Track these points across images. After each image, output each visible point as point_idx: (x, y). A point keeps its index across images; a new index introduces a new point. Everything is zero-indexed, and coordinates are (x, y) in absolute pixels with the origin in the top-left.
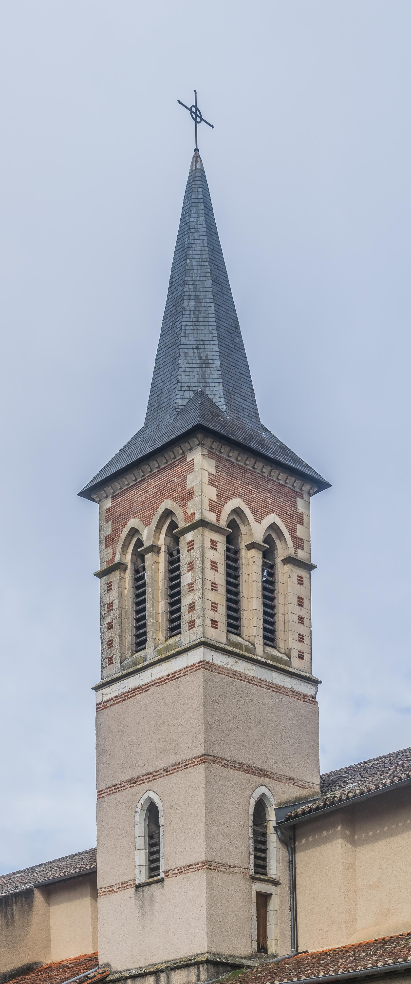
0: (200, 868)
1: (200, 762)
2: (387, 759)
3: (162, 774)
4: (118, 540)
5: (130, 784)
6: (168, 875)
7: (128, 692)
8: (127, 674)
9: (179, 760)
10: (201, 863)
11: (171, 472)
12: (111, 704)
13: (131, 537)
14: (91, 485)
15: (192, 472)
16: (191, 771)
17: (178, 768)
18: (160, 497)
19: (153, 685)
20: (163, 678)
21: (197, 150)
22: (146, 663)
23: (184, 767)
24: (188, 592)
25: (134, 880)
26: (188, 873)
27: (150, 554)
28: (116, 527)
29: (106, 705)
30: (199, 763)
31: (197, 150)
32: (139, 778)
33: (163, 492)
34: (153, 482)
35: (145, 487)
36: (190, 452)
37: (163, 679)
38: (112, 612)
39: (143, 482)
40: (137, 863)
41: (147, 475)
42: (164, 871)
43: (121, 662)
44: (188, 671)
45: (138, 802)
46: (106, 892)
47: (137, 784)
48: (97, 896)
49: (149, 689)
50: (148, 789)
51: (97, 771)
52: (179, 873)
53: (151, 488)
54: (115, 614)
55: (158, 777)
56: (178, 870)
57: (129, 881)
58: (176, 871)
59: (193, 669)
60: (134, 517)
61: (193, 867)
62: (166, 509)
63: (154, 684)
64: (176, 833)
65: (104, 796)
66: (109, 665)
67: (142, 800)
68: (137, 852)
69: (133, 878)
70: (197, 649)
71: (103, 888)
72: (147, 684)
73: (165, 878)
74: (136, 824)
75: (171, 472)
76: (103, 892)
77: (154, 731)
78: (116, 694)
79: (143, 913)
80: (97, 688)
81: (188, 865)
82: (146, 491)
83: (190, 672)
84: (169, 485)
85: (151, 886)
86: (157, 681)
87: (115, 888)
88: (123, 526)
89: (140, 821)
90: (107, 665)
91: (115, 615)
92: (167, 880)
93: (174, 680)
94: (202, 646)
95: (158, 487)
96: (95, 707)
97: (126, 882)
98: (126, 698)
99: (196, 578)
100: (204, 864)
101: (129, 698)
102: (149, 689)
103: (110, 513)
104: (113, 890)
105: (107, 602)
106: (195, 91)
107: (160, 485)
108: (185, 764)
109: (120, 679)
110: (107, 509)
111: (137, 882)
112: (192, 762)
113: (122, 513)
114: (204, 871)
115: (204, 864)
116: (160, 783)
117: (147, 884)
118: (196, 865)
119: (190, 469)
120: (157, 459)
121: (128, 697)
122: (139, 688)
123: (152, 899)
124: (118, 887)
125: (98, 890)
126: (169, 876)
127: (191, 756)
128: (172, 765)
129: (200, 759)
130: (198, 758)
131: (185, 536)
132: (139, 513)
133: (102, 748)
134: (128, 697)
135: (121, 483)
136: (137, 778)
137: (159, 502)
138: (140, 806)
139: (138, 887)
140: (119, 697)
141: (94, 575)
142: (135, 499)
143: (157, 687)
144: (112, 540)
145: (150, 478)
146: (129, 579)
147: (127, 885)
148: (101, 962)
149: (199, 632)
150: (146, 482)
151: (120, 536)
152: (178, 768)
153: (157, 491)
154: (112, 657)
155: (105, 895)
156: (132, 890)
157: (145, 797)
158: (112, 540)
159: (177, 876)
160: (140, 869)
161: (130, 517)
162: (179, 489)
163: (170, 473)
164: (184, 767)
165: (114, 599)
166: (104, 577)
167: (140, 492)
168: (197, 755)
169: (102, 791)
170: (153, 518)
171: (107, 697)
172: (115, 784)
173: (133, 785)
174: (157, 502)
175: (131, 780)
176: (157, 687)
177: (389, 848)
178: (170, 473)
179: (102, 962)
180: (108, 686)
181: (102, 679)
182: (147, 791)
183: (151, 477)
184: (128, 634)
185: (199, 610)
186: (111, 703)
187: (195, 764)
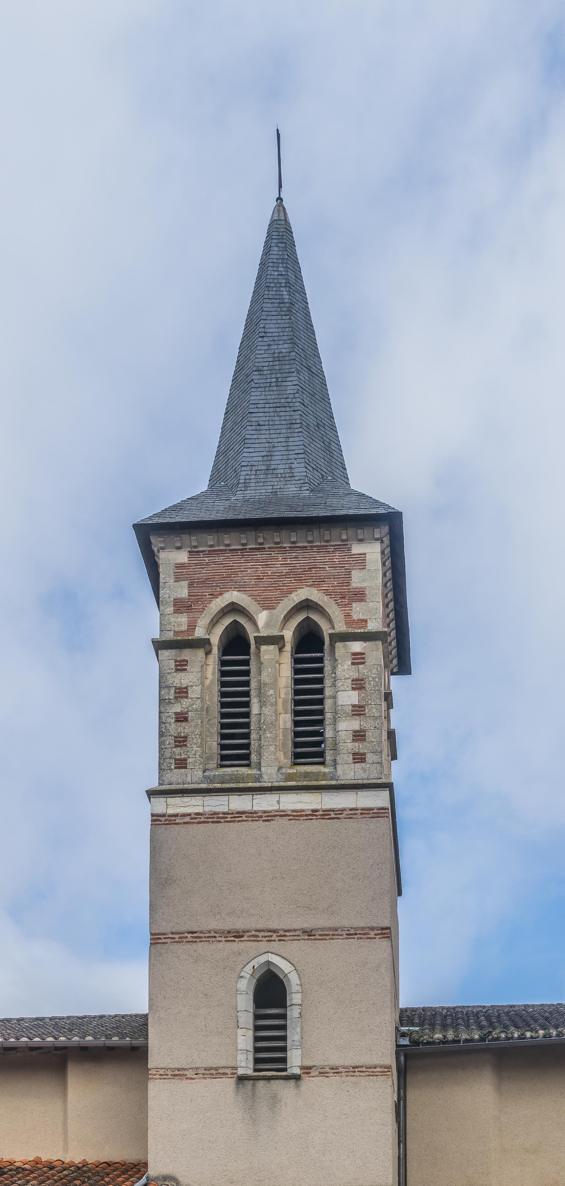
0: (378, 1074)
1: (380, 936)
2: (42, 1024)
3: (298, 936)
4: (202, 610)
5: (227, 937)
6: (310, 1073)
7: (224, 813)
8: (192, 789)
9: (337, 925)
10: (381, 1067)
11: (319, 557)
12: (185, 820)
13: (222, 614)
14: (156, 521)
15: (363, 569)
16: (362, 944)
17: (333, 935)
18: (294, 580)
19: (281, 816)
20: (303, 811)
21: (279, 199)
22: (257, 785)
23: (345, 936)
24: (353, 715)
25: (236, 1068)
26: (351, 1076)
27: (272, 647)
28: (194, 593)
29: (175, 820)
30: (378, 937)
31: (279, 199)
32: (248, 932)
33: (302, 577)
34: (281, 558)
35: (262, 560)
36: (360, 544)
37: (304, 813)
38: (186, 700)
39: (259, 552)
40: (240, 1047)
41: (268, 546)
42: (300, 1065)
43: (204, 772)
44: (357, 814)
45: (246, 964)
46: (167, 1075)
47: (242, 939)
48: (147, 1080)
49: (272, 820)
50: (268, 950)
51: (151, 905)
52: (333, 1073)
53: (277, 564)
54: (193, 705)
55: (288, 938)
56: (332, 1069)
57: (223, 1067)
58: (327, 1070)
59: (369, 814)
60: (238, 591)
61: (364, 1069)
62: (307, 600)
63: (282, 814)
64: (329, 1019)
65: (167, 943)
66: (176, 768)
67: (256, 963)
68: (240, 1032)
69: (233, 1065)
70: (376, 791)
71: (162, 1069)
72: (270, 812)
73: (302, 1075)
74: (239, 992)
75: (319, 557)
76: (161, 1075)
77: (284, 876)
78: (200, 810)
79: (254, 1117)
80: (151, 794)
81: (353, 1065)
82: (265, 565)
83: (361, 816)
84: (314, 571)
85: (272, 1082)
86: (289, 813)
87: (190, 1074)
88: (214, 596)
89: (248, 991)
90: (173, 767)
91: (194, 707)
92: (306, 1079)
93: (328, 819)
94: (388, 789)
95: (290, 567)
96: (150, 818)
97: (216, 1069)
98: (222, 820)
99: (370, 702)
100: (387, 1070)
101: (225, 822)
102: (272, 820)
103: (184, 571)
104: (186, 1075)
105: (175, 685)
106: (278, 130)
107: (296, 566)
108: (348, 932)
109: (209, 793)
110: (179, 564)
111: (241, 1072)
112: (364, 932)
113: (213, 578)
114: (388, 1078)
115: (387, 1070)
116: (293, 948)
117: (267, 1078)
118: (370, 1068)
119: (357, 564)
120: (314, 530)
121: (226, 820)
122: (251, 813)
123: (274, 1100)
124: (196, 1072)
125: (148, 1070)
126: (311, 1075)
127: (362, 925)
128: (322, 929)
129: (380, 932)
130: (378, 930)
131: (348, 643)
132: (250, 589)
133: (165, 876)
134: (226, 820)
135: (216, 538)
136: (244, 932)
137: (292, 586)
138: (249, 969)
139: (242, 1079)
140: (205, 816)
141: (153, 642)
142: (241, 569)
143: (289, 820)
144: (189, 607)
145: (275, 551)
146: (214, 669)
147: (216, 1072)
148: (153, 1171)
149: (375, 771)
150: (264, 553)
151: (206, 606)
152: (333, 935)
153: (288, 571)
154: (185, 760)
155: (164, 1079)
156: (233, 1081)
157: (263, 959)
158: (189, 607)
159: (328, 1077)
160: (247, 1056)
161: (231, 588)
162: (336, 583)
163: (317, 557)
164: (345, 936)
165: (191, 684)
166: (170, 651)
167: (252, 562)
168: (375, 925)
169: (164, 934)
170: (279, 603)
171: (175, 810)
172: (192, 930)
173: (233, 939)
174: (290, 586)
175: (229, 932)
176: (289, 820)
177: (557, 1109)
178: (317, 557)
179: (157, 1173)
180: (181, 795)
181: (160, 784)
182: (266, 953)
183: (276, 550)
184: (210, 739)
185: (375, 743)
186: (187, 819)
187: (369, 936)
